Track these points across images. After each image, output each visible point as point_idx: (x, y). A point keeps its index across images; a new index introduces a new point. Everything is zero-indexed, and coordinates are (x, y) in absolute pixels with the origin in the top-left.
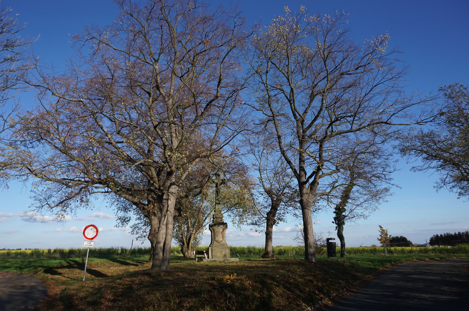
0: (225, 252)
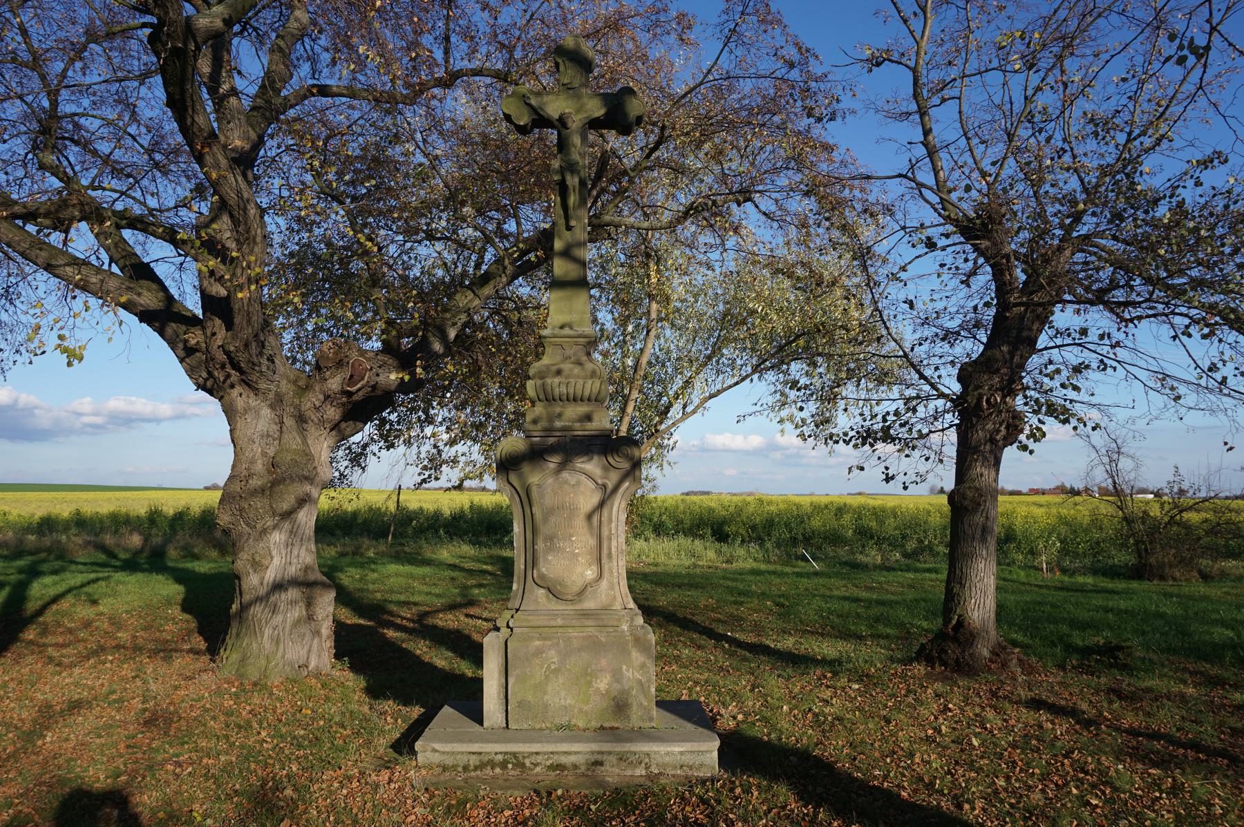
0: (617, 676)
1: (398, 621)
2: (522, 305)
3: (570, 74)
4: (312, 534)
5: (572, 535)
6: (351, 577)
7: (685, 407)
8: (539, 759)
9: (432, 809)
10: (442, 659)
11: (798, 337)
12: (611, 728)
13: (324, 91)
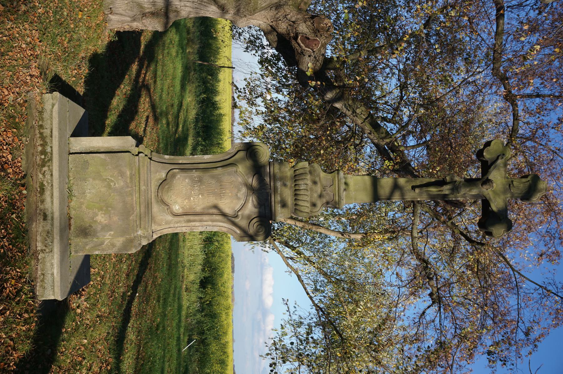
0: (106, 228)
1: (143, 71)
2: (359, 148)
3: (520, 185)
4: (201, 15)
5: (202, 195)
6: (173, 36)
7: (291, 258)
8: (48, 177)
9: (12, 106)
10: (118, 102)
11: (340, 335)
12: (70, 225)
13: (500, 16)
